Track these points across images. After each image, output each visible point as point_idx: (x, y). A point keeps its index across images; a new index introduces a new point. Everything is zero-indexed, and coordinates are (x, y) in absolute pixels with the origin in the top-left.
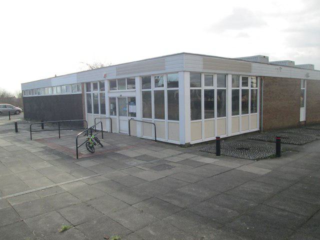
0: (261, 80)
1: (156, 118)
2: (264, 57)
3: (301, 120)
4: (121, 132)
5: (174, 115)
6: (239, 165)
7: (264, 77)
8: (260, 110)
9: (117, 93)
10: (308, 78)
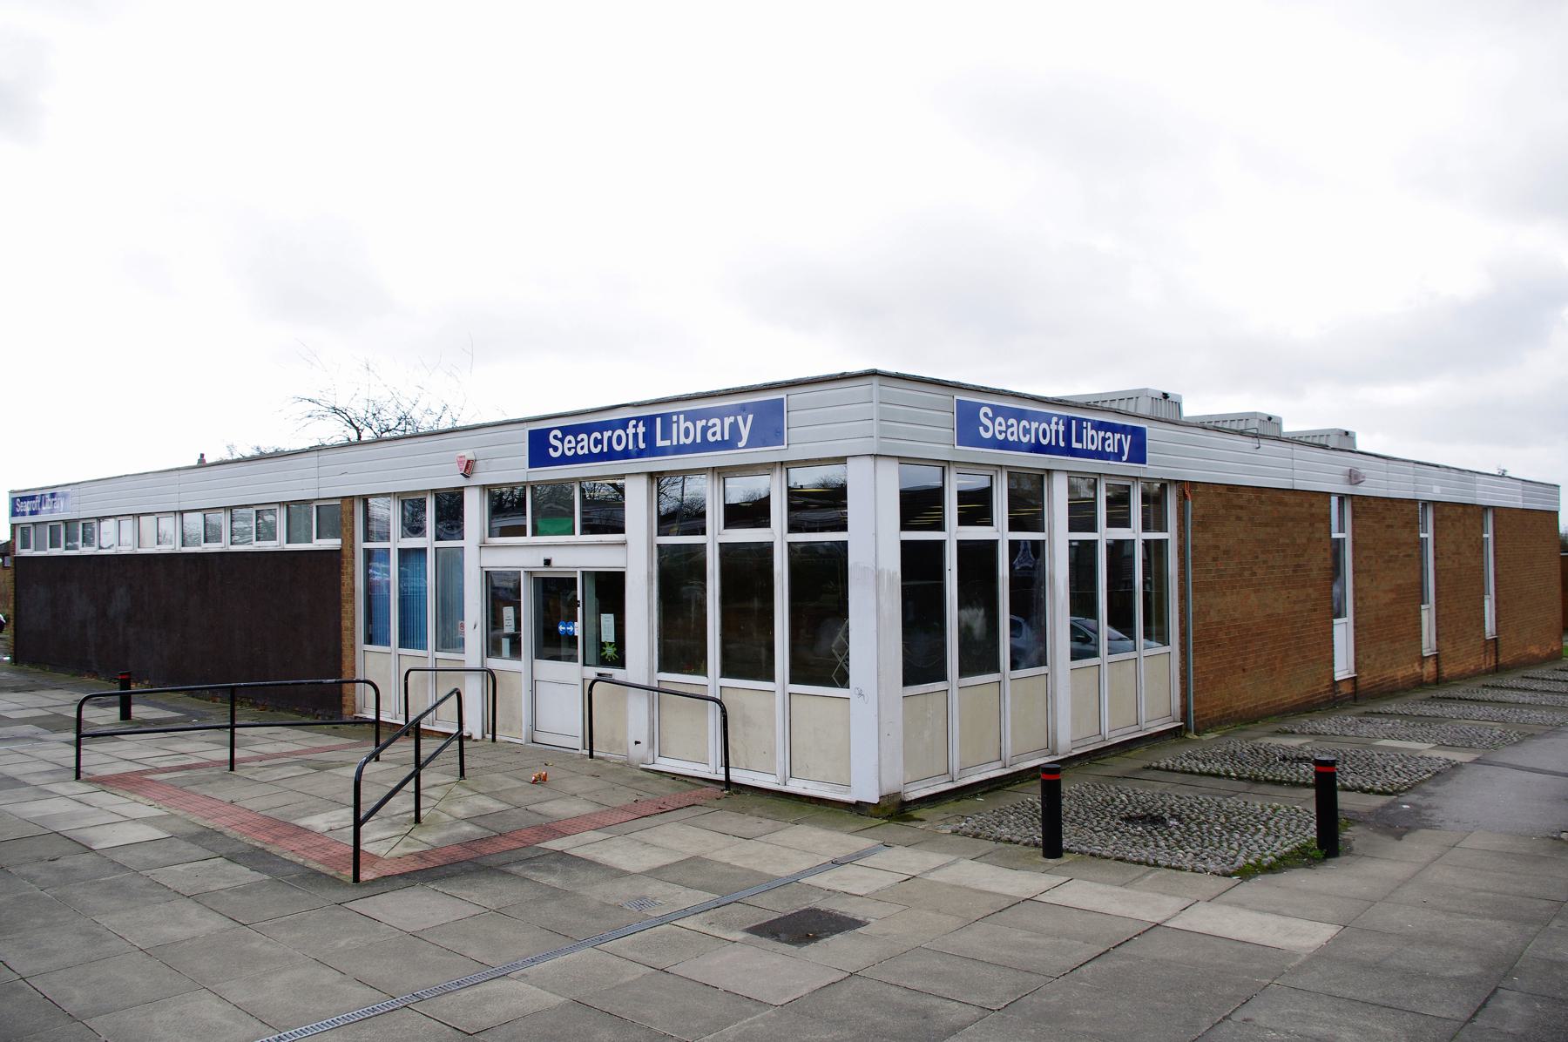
0: (1183, 498)
1: (726, 672)
2: (1166, 396)
3: (1339, 676)
4: (539, 737)
5: (822, 663)
6: (1172, 904)
7: (1194, 484)
8: (1183, 634)
9: (524, 555)
10: (1362, 490)
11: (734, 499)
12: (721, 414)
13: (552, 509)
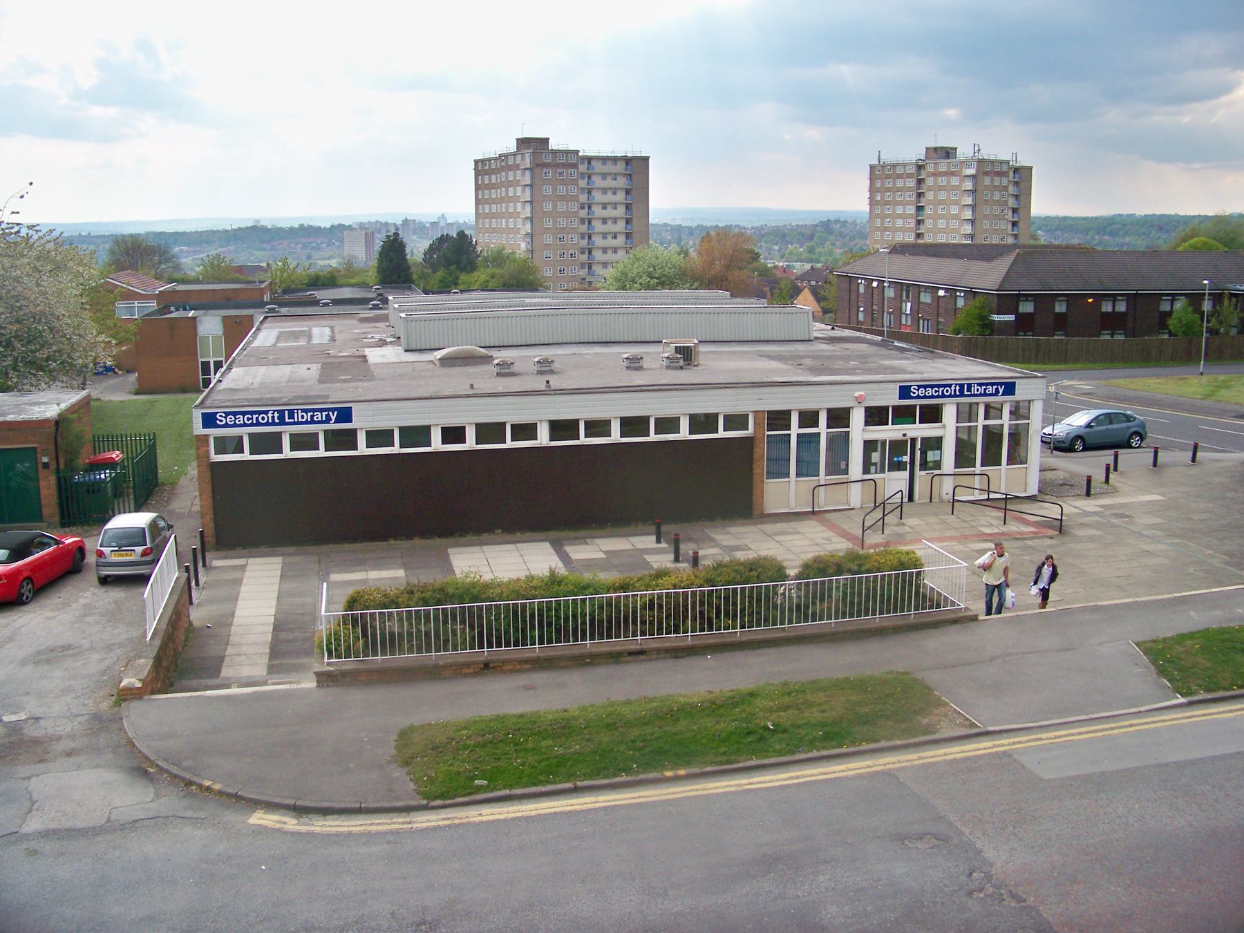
11: (433, 430)
12: (992, 384)
13: (903, 414)
